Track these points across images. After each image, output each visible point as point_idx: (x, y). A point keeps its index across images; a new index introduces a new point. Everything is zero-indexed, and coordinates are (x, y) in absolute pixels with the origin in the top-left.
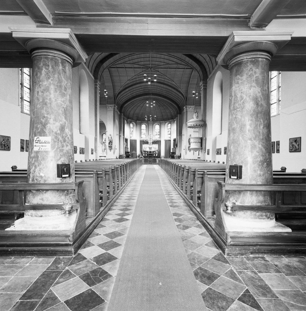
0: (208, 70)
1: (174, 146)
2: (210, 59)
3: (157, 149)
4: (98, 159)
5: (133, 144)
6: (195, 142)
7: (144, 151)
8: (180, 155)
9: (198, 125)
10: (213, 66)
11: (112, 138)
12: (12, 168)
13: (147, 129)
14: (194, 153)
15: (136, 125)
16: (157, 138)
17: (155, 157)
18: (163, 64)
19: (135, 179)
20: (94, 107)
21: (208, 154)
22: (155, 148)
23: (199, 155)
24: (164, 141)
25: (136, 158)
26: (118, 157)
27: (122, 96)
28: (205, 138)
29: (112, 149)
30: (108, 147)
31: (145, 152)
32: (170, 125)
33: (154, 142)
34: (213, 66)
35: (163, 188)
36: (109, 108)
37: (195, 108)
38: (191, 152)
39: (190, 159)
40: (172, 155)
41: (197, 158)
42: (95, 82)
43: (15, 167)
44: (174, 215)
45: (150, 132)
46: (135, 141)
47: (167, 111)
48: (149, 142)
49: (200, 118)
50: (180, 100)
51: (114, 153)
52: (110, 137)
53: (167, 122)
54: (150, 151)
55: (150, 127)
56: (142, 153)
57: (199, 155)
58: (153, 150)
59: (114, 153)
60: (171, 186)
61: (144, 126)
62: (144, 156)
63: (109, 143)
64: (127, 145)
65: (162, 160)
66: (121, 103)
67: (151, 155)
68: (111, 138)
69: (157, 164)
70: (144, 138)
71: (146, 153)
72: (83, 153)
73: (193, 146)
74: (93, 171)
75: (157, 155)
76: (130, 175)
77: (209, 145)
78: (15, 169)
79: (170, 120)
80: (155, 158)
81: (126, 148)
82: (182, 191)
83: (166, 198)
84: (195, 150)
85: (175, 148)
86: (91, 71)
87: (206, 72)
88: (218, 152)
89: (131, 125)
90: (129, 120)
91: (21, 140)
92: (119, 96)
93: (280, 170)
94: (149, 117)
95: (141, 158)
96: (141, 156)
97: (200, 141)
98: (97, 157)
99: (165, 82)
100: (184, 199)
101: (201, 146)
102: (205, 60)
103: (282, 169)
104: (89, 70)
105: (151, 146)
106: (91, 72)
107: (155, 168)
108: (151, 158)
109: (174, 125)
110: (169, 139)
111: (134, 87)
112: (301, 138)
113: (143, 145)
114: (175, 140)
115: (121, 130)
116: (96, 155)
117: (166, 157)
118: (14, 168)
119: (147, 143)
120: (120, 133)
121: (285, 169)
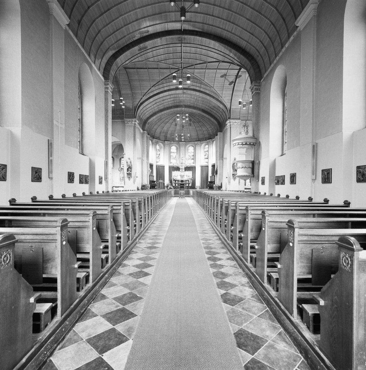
0: (262, 66)
1: (213, 173)
3: (191, 177)
4: (110, 190)
5: (160, 171)
6: (244, 167)
7: (174, 180)
8: (220, 185)
10: (270, 60)
12: (32, 199)
13: (178, 151)
14: (239, 183)
15: (164, 146)
16: (190, 163)
17: (188, 187)
18: (199, 62)
19: (157, 223)
20: (104, 119)
21: (263, 183)
22: (188, 175)
23: (245, 185)
24: (200, 167)
25: (164, 188)
26: (140, 188)
27: (145, 109)
28: (257, 162)
29: (131, 177)
30: (126, 175)
31: (175, 181)
32: (207, 146)
33: (187, 169)
34: (270, 60)
35: (203, 243)
36: (127, 123)
37: (241, 123)
39: (232, 190)
40: (210, 185)
42: (105, 85)
43: (14, 200)
44: (240, 345)
45: (181, 154)
46: (163, 167)
48: (181, 167)
49: (250, 134)
51: (134, 182)
52: (129, 161)
53: (203, 143)
54: (182, 179)
55: (182, 149)
56: (171, 182)
57: (245, 185)
58: (185, 178)
59: (134, 182)
60: (209, 227)
61: (174, 149)
62: (173, 187)
63: (128, 169)
64: (152, 172)
65: (197, 192)
66: (145, 118)
67: (183, 184)
68: (131, 162)
69: (191, 197)
70: (174, 163)
71: (177, 182)
72: (87, 182)
73: (240, 172)
74: (120, 203)
75: (190, 185)
76: (160, 207)
77: (264, 171)
78: (52, 199)
79: (208, 141)
80: (188, 188)
81: (151, 175)
82: (208, 216)
83: (199, 235)
84: (244, 177)
85: (215, 176)
86: (100, 68)
88: (278, 181)
89: (158, 147)
91: (33, 168)
92: (141, 108)
93: (342, 204)
94: (180, 136)
95: (170, 188)
96: (170, 186)
97: (251, 165)
98: (107, 187)
99: (202, 90)
100: (249, 278)
101: (253, 172)
102: (259, 53)
104: (96, 66)
105: (182, 174)
106: (99, 70)
107: (188, 203)
108: (182, 188)
110: (206, 164)
112: (331, 169)
113: (173, 172)
114: (213, 166)
116: (106, 185)
117: (202, 187)
118: (34, 199)
119: (178, 169)
120: (143, 156)
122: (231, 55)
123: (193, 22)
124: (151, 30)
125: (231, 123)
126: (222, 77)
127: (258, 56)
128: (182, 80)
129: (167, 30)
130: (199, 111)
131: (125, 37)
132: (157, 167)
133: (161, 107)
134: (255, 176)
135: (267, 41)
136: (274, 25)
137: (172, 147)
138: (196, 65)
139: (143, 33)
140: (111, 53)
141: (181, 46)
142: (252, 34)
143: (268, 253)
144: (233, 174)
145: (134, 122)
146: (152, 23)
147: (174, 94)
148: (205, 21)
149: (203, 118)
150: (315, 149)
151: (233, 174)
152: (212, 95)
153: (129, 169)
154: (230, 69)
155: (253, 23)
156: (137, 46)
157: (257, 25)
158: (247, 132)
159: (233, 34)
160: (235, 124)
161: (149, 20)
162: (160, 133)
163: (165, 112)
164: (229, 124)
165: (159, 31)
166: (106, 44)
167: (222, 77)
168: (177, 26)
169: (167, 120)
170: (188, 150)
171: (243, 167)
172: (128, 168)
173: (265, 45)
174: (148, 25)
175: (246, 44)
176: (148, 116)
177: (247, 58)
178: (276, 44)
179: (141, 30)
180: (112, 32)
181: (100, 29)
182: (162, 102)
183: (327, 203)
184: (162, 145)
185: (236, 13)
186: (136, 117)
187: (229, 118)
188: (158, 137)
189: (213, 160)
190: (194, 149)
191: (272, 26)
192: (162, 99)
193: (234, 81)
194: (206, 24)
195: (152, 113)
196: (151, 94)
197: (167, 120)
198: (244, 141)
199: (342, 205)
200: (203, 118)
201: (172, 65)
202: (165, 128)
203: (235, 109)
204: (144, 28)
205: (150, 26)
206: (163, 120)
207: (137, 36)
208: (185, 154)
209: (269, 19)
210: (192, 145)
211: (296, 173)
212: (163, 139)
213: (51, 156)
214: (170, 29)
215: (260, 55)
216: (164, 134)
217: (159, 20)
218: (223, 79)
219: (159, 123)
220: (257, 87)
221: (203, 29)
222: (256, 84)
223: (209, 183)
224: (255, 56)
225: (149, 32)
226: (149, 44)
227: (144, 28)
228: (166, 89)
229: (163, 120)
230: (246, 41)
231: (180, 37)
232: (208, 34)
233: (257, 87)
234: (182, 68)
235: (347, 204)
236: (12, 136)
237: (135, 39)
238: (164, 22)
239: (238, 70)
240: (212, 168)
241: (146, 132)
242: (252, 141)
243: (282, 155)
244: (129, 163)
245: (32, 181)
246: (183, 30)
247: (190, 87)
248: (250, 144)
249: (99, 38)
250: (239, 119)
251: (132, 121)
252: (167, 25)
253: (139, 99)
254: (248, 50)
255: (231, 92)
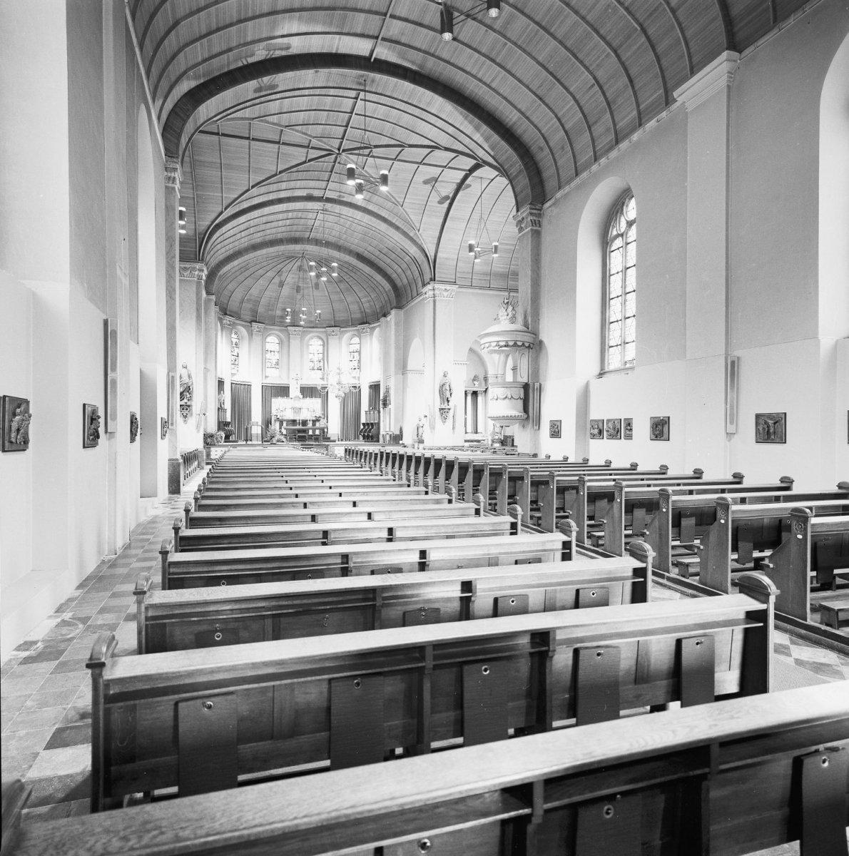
2: (569, 139)
8: (398, 433)
9: (520, 344)
11: (193, 376)
13: (285, 350)
15: (251, 334)
16: (314, 379)
18: (386, 141)
22: (309, 409)
28: (537, 385)
29: (192, 414)
33: (308, 392)
38: (446, 424)
41: (461, 443)
42: (166, 169)
47: (349, 299)
50: (404, 266)
55: (295, 343)
68: (189, 376)
70: (275, 378)
87: (541, 183)
90: (228, 318)
93: (562, 459)
101: (526, 409)
103: (695, 472)
105: (298, 404)
109: (371, 343)
111: (267, 210)
112: (785, 414)
114: (375, 388)
115: (209, 350)
119: (283, 391)
121: (742, 477)
122: (477, 137)
123: (404, 45)
124: (298, 46)
125: (437, 292)
126: (426, 182)
127: (541, 149)
128: (362, 182)
129: (334, 52)
130: (349, 255)
131: (230, 50)
132: (233, 385)
133: (258, 238)
134: (531, 417)
135: (574, 118)
136: (601, 88)
137: (269, 339)
138: (376, 147)
139: (275, 50)
140: (186, 86)
141: (356, 98)
142: (540, 99)
143: (578, 591)
144: (441, 409)
145: (196, 273)
146: (304, 29)
147: (299, 210)
148: (433, 50)
149: (352, 274)
150: (733, 369)
151: (441, 409)
152: (394, 222)
153: (185, 393)
154: (450, 168)
155: (551, 73)
156: (255, 81)
157: (558, 80)
158: (513, 320)
159: (493, 90)
160: (445, 294)
161: (300, 19)
162: (242, 302)
163: (264, 251)
164: (431, 293)
165: (314, 50)
166: (181, 62)
167: (426, 182)
168: (361, 47)
169: (261, 272)
170: (308, 345)
171: (506, 397)
172: (182, 390)
173: (567, 127)
174: (294, 31)
175: (519, 118)
176: (221, 257)
177: (515, 149)
178: (598, 129)
179: (273, 41)
180: (204, 31)
181: (177, 18)
182: (263, 227)
183: (567, 461)
184: (243, 331)
185: (515, 44)
186: (203, 259)
187: (431, 280)
188: (236, 313)
189: (372, 372)
190: (323, 345)
191: (596, 88)
192: (264, 219)
193: (451, 196)
194: (433, 55)
195: (231, 252)
196: (245, 205)
197: (261, 272)
198: (509, 338)
199: (731, 481)
200: (352, 274)
201: (318, 140)
202: (254, 292)
203: (446, 259)
204: (283, 36)
205: (298, 36)
206: (252, 270)
207: (260, 54)
208: (302, 356)
209: (591, 73)
210: (317, 334)
211: (669, 417)
212: (248, 318)
213: (114, 369)
214: (343, 50)
215: (549, 146)
216: (250, 306)
217: (324, 23)
218: (429, 187)
219: (241, 278)
220: (535, 218)
221: (421, 66)
222: (534, 211)
223: (362, 427)
224: (534, 149)
225: (290, 50)
226: (284, 79)
227: (283, 36)
228: (283, 195)
229: (252, 270)
230: (519, 111)
231: (362, 76)
232: (432, 79)
233: (535, 218)
234: (339, 150)
235: (698, 474)
236: (37, 310)
237: (251, 60)
238: (334, 31)
239: (464, 173)
240: (370, 393)
241: (213, 297)
242: (527, 338)
243: (601, 375)
244: (185, 379)
245: (84, 447)
246: (372, 60)
247: (344, 197)
248: (515, 345)
249: (172, 42)
250: (455, 283)
251: (194, 269)
252: (340, 39)
253: (216, 214)
254: (519, 131)
255: (441, 221)
